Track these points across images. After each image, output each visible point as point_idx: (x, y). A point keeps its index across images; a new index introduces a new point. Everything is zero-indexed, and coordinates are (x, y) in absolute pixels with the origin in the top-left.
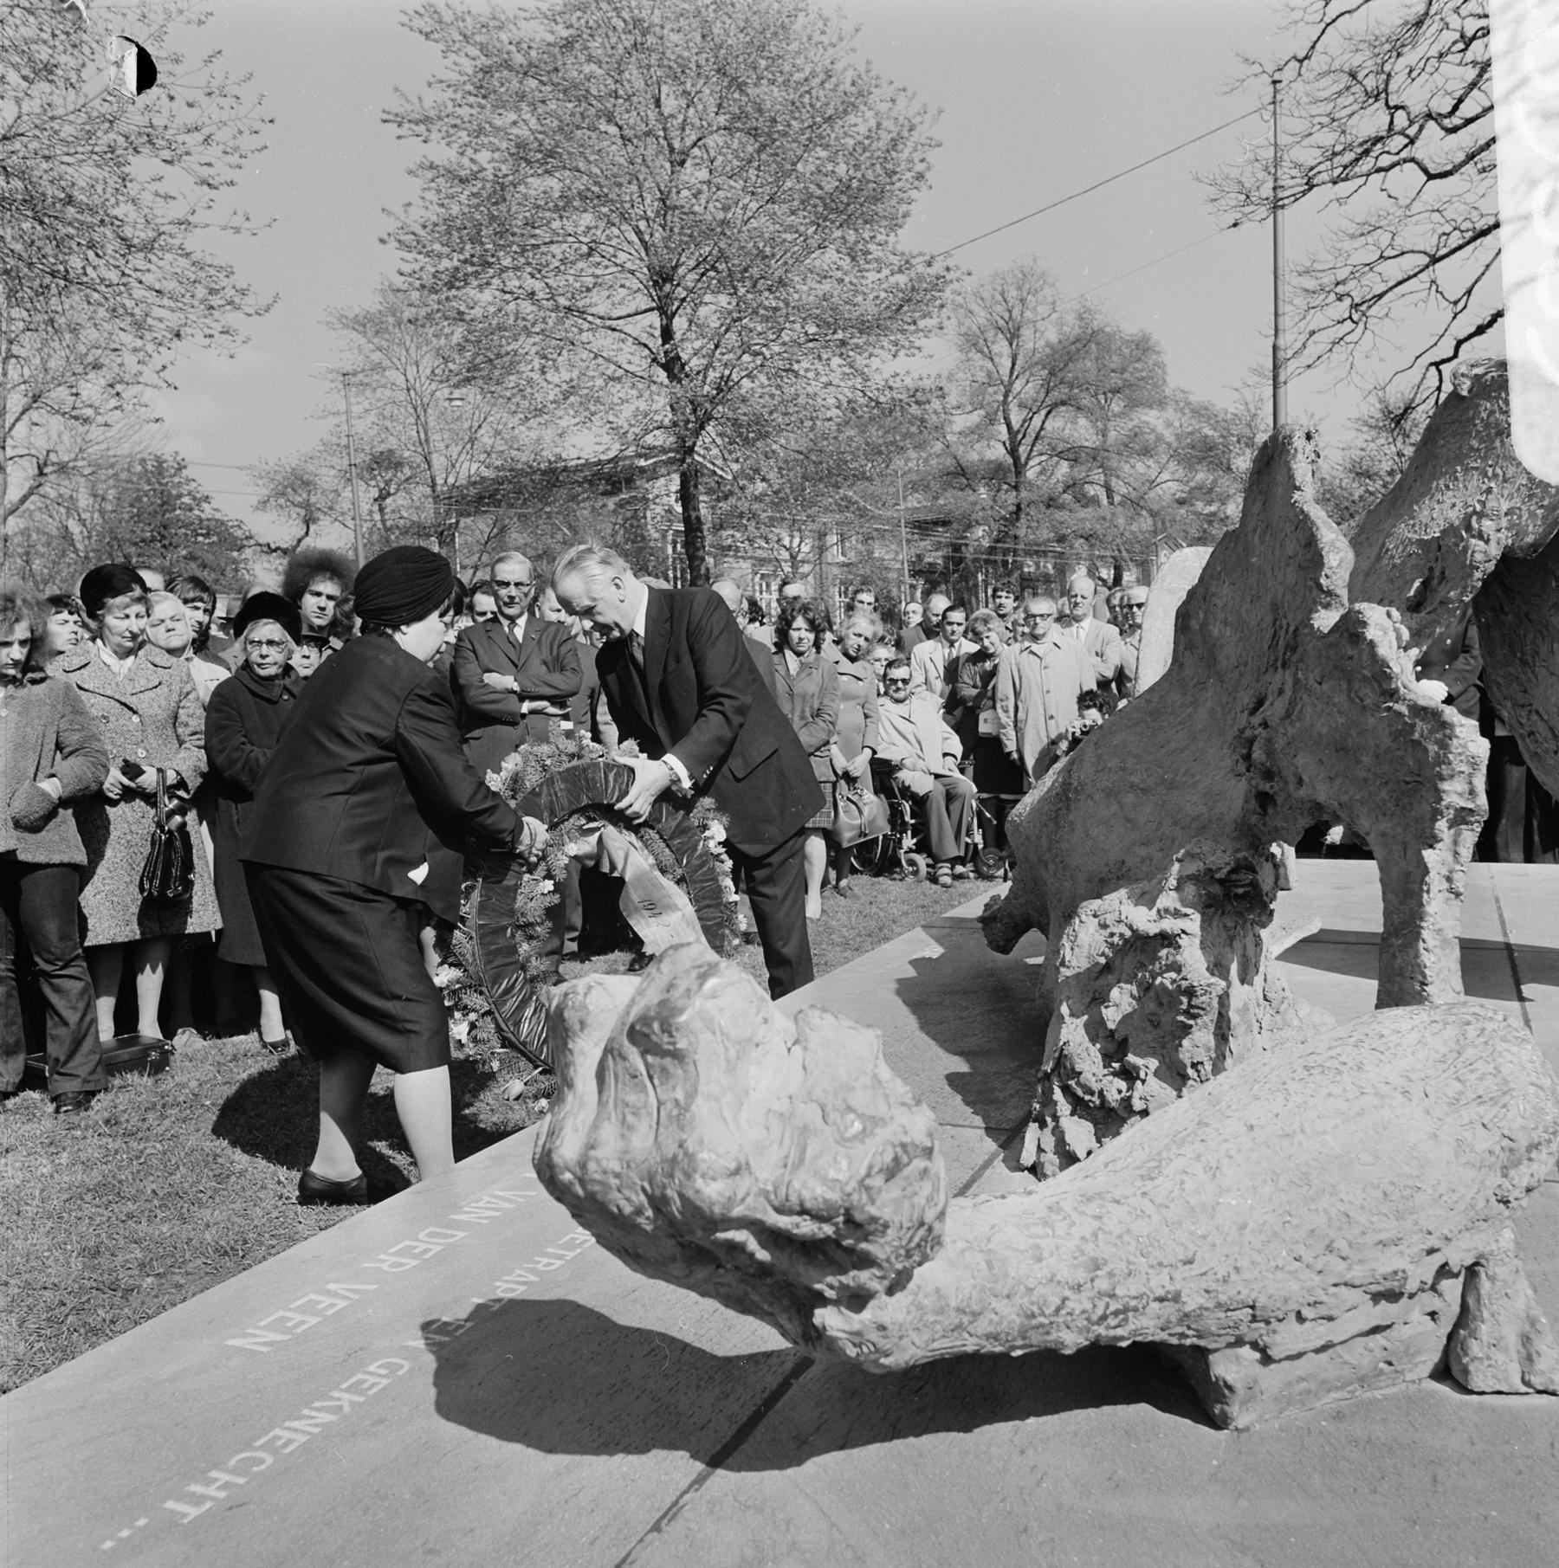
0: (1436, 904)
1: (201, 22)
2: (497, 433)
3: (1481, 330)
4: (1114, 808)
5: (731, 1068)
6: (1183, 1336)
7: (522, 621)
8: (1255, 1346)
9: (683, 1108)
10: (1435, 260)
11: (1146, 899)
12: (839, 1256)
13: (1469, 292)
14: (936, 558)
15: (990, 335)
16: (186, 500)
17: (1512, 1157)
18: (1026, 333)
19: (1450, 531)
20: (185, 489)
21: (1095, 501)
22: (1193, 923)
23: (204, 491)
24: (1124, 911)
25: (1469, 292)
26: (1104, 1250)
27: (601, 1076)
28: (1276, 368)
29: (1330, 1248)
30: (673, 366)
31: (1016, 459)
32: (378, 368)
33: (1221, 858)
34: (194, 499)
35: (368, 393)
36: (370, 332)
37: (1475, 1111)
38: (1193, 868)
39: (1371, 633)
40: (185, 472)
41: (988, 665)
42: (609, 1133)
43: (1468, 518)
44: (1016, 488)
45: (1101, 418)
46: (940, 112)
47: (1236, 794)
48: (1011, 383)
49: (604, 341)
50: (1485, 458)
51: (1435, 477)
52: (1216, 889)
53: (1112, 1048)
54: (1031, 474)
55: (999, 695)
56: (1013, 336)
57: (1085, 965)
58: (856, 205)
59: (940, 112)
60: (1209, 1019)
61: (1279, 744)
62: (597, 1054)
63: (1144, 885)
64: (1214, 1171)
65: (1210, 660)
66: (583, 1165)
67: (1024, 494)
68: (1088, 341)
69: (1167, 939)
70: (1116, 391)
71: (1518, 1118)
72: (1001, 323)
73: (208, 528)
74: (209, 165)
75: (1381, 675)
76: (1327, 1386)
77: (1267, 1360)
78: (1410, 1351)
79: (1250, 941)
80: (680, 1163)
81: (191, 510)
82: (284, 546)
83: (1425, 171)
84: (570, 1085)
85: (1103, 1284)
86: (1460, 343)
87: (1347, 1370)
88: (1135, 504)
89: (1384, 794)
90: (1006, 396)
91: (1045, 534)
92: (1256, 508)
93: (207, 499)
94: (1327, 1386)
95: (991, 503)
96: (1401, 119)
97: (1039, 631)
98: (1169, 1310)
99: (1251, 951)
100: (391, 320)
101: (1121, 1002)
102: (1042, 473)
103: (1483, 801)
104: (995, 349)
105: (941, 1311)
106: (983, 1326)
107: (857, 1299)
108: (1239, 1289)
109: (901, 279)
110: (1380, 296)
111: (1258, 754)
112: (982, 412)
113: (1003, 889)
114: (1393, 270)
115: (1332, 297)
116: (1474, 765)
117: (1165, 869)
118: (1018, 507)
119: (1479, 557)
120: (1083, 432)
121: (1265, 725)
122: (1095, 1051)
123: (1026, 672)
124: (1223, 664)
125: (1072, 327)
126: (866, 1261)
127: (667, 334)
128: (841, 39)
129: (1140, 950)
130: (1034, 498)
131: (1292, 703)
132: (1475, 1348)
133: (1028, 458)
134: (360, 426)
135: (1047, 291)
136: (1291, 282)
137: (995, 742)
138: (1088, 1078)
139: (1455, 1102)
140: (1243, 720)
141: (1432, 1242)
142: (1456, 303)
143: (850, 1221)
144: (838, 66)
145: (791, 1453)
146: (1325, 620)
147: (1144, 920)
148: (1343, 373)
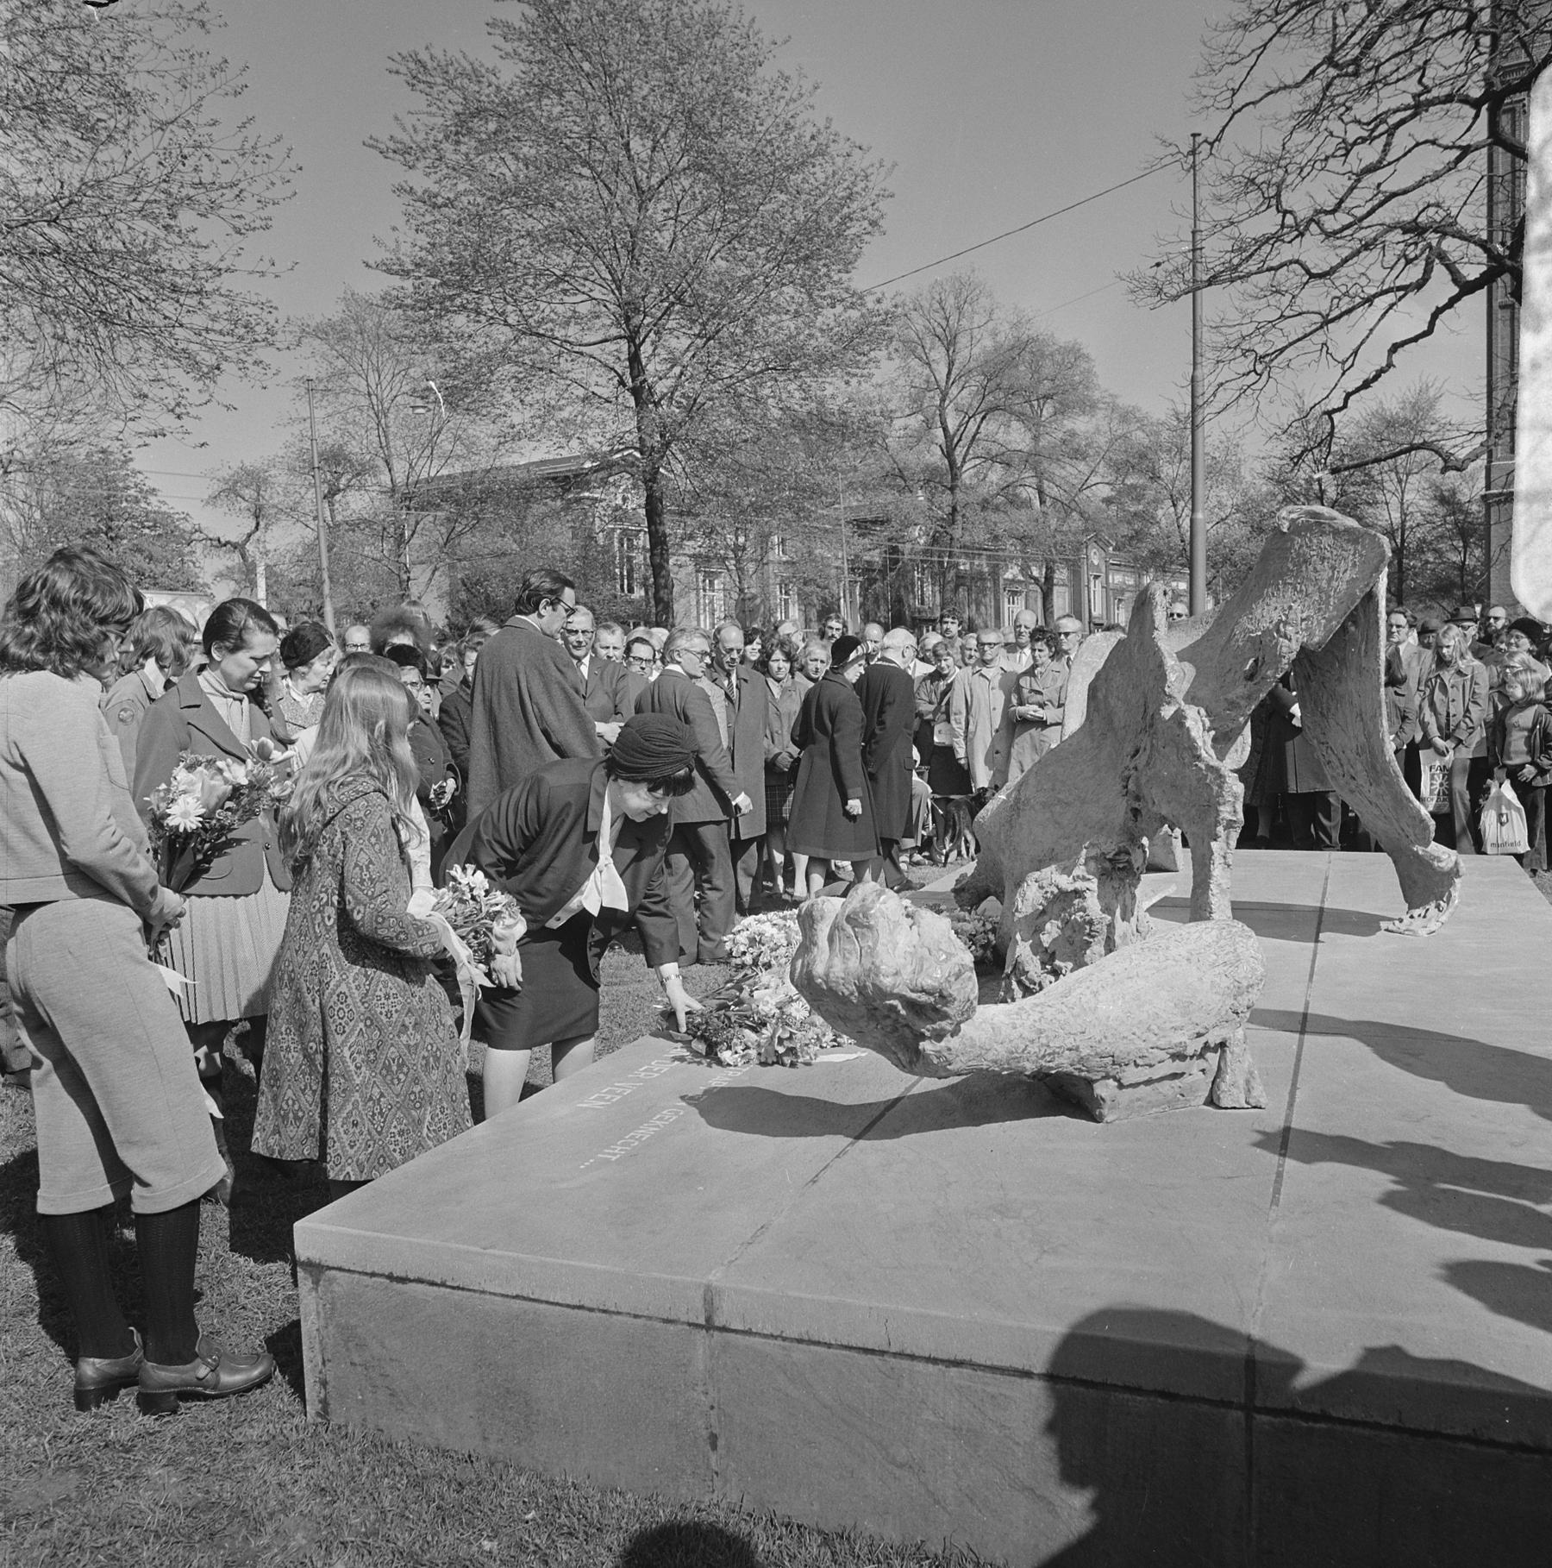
0: (1217, 870)
1: (236, 93)
2: (457, 438)
3: (1366, 384)
4: (1048, 815)
5: (891, 933)
6: (1080, 1070)
7: (586, 660)
8: (1115, 1079)
9: (872, 949)
10: (1327, 321)
11: (1067, 871)
12: (931, 1014)
13: (1355, 353)
14: (876, 556)
15: (928, 342)
16: (132, 492)
17: (1239, 992)
18: (963, 341)
19: (1266, 632)
20: (131, 482)
21: (1027, 504)
22: (1094, 884)
23: (150, 484)
24: (1054, 878)
25: (1355, 353)
26: (1045, 1026)
27: (831, 940)
28: (1194, 410)
29: (1149, 1029)
30: (641, 394)
31: (952, 464)
32: (342, 374)
33: (1110, 848)
34: (141, 491)
35: (331, 398)
36: (332, 338)
37: (1221, 969)
38: (1093, 853)
39: (1188, 723)
40: (131, 465)
41: (942, 685)
42: (837, 961)
43: (1277, 625)
44: (952, 489)
45: (1032, 422)
46: (895, 165)
47: (1122, 807)
48: (948, 388)
49: (579, 370)
50: (1296, 577)
51: (1266, 586)
52: (1107, 865)
53: (1046, 958)
54: (967, 476)
55: (953, 709)
56: (950, 344)
57: (1030, 911)
58: (815, 246)
59: (895, 165)
60: (1101, 938)
61: (1143, 781)
62: (827, 930)
63: (1067, 863)
64: (1095, 994)
65: (1109, 720)
66: (827, 975)
67: (959, 495)
68: (1023, 349)
69: (1078, 893)
70: (1046, 397)
71: (1242, 972)
72: (939, 330)
73: (155, 521)
74: (240, 217)
75: (1192, 747)
76: (1152, 1105)
77: (1121, 1086)
78: (1193, 1089)
79: (1128, 895)
80: (874, 970)
81: (137, 502)
82: (234, 540)
83: (1308, 271)
84: (815, 944)
85: (1044, 1041)
86: (1348, 395)
87: (1161, 1097)
88: (1067, 508)
89: (1193, 811)
90: (943, 400)
91: (981, 536)
92: (1136, 630)
93: (153, 491)
94: (1152, 1105)
95: (927, 504)
96: (1289, 220)
97: (988, 657)
98: (1074, 1054)
99: (1128, 902)
100: (353, 328)
101: (1051, 931)
102: (976, 475)
103: (1241, 816)
104: (933, 355)
105: (973, 1046)
106: (990, 1056)
107: (939, 1036)
108: (1105, 1048)
109: (854, 314)
110: (1282, 351)
111: (1131, 786)
112: (921, 417)
113: (970, 868)
114: (1295, 327)
115: (1238, 352)
116: (1236, 797)
117: (1078, 853)
118: (954, 509)
119: (1284, 650)
120: (1017, 437)
121: (1136, 768)
122: (1037, 960)
123: (978, 691)
124: (1116, 724)
125: (1006, 336)
126: (946, 1016)
127: (634, 359)
128: (801, 95)
129: (1065, 898)
130: (970, 500)
131: (1150, 757)
132: (1223, 1086)
133: (964, 461)
134: (323, 430)
135: (983, 300)
136: (1206, 336)
137: (949, 750)
138: (1032, 975)
139: (1213, 965)
140: (1127, 761)
141: (1200, 1029)
142: (1344, 363)
143: (941, 996)
144: (799, 121)
145: (896, 1133)
146: (1167, 712)
147: (1066, 882)
148: (1250, 416)
